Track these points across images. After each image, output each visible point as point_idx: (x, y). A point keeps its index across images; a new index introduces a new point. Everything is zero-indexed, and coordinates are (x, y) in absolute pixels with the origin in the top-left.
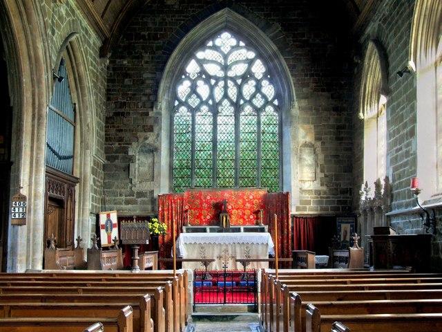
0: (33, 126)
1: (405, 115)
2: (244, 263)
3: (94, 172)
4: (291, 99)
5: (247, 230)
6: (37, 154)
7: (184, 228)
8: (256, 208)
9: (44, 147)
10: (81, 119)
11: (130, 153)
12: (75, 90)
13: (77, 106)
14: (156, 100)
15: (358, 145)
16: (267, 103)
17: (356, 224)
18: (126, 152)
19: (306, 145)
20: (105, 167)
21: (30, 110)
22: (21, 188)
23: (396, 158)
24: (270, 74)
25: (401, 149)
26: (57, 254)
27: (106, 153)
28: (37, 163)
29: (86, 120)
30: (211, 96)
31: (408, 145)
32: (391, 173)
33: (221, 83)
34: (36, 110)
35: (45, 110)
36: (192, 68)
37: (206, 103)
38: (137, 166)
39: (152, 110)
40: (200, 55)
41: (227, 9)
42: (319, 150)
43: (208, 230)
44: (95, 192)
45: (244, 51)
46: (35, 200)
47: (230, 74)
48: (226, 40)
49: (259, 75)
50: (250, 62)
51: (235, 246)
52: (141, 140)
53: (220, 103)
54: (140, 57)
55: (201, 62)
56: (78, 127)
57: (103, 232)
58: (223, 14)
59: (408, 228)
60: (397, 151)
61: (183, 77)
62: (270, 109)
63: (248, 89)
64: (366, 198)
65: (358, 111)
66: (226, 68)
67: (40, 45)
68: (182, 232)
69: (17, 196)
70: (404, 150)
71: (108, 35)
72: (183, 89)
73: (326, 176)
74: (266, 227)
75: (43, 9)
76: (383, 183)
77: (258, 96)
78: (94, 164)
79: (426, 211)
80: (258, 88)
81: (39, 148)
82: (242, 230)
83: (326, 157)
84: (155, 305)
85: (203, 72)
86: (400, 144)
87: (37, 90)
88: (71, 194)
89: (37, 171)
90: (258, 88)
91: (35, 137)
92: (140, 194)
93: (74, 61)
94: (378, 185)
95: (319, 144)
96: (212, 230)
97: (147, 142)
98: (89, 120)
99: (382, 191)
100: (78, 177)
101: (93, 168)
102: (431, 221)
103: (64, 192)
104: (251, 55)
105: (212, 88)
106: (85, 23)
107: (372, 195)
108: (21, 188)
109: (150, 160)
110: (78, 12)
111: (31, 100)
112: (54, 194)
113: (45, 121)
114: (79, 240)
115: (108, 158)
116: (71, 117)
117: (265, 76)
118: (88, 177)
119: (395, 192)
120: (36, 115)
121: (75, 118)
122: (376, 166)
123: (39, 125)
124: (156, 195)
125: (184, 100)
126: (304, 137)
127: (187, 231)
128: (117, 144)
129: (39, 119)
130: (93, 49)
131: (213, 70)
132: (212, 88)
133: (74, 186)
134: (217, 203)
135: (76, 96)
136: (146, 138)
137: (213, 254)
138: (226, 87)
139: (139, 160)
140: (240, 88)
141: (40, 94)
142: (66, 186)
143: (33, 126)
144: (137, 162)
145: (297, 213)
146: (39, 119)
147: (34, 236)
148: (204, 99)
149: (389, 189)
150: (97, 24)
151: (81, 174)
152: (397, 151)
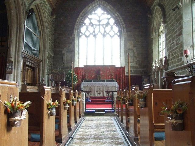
2: (108, 93)
5: (107, 81)
6: (19, 44)
8: (111, 73)
10: (43, 37)
11: (63, 52)
12: (40, 25)
13: (41, 31)
15: (150, 49)
17: (150, 79)
19: (130, 49)
20: (53, 58)
21: (16, 25)
22: (11, 58)
23: (171, 48)
24: (117, 23)
27: (54, 52)
29: (45, 37)
30: (94, 32)
31: (179, 39)
33: (98, 27)
34: (19, 25)
36: (87, 21)
38: (66, 57)
40: (90, 16)
42: (135, 51)
45: (106, 15)
46: (17, 63)
47: (101, 23)
48: (99, 11)
50: (109, 19)
51: (103, 88)
55: (90, 19)
57: (50, 81)
61: (83, 25)
64: (156, 67)
65: (150, 35)
66: (99, 21)
70: (175, 43)
71: (55, 7)
73: (138, 61)
74: (115, 80)
76: (164, 59)
78: (49, 55)
80: (112, 28)
85: (91, 23)
86: (173, 41)
90: (112, 28)
93: (39, 13)
95: (135, 49)
97: (69, 48)
98: (46, 38)
99: (164, 62)
100: (42, 59)
101: (48, 57)
102: (194, 69)
104: (109, 16)
108: (11, 58)
111: (16, 21)
115: (55, 54)
117: (114, 24)
119: (169, 62)
120: (19, 27)
122: (161, 50)
126: (129, 46)
127: (85, 82)
130: (48, 11)
135: (41, 28)
136: (69, 47)
137: (95, 90)
139: (66, 55)
143: (17, 32)
144: (66, 56)
146: (20, 29)
148: (91, 33)
149: (167, 61)
150: (51, 4)
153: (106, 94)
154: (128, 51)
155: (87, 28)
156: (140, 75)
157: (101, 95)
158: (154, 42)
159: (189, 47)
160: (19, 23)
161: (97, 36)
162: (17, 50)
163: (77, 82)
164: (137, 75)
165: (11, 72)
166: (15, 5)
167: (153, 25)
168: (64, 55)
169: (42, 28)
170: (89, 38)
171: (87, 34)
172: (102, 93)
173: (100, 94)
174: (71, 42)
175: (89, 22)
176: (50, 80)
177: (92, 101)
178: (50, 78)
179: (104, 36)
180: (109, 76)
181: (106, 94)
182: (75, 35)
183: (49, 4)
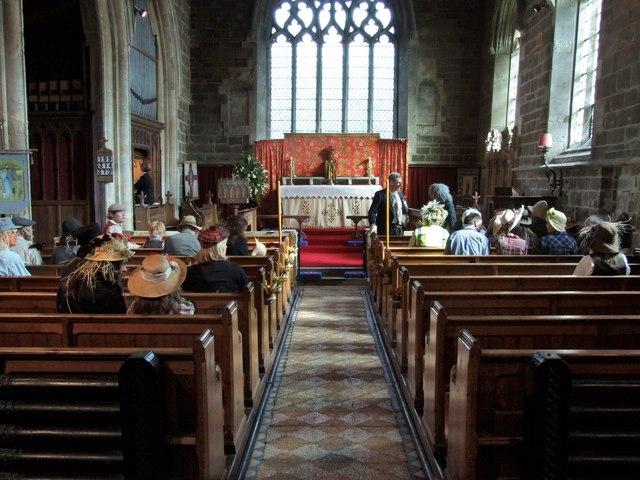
0: (114, 69)
1: (542, 68)
3: (180, 116)
6: (121, 102)
7: (284, 179)
9: (127, 93)
10: (163, 54)
11: (221, 92)
14: (249, 28)
16: (382, 31)
18: (216, 91)
19: (425, 83)
22: (105, 141)
25: (533, 96)
26: (149, 214)
28: (121, 112)
29: (169, 53)
30: (316, 22)
32: (520, 123)
34: (117, 51)
35: (127, 50)
37: (309, 30)
39: (245, 40)
43: (312, 182)
46: (121, 154)
53: (325, 31)
56: (160, 63)
59: (534, 186)
60: (529, 98)
62: (384, 38)
65: (488, 45)
68: (282, 184)
69: (102, 150)
73: (448, 120)
74: (377, 179)
77: (372, 22)
79: (553, 170)
81: (121, 95)
82: (350, 182)
84: (357, 377)
87: (115, 27)
88: (157, 143)
92: (234, 140)
94: (505, 134)
96: (316, 182)
97: (241, 78)
103: (148, 141)
105: (316, 12)
107: (497, 146)
108: (105, 141)
109: (244, 100)
111: (109, 39)
112: (142, 146)
113: (127, 63)
116: (153, 54)
118: (174, 122)
121: (154, 53)
123: (120, 69)
124: (251, 142)
125: (282, 26)
127: (288, 183)
128: (205, 81)
132: (316, 12)
133: (159, 133)
134: (325, 150)
135: (156, 26)
136: (239, 74)
140: (349, 11)
141: (120, 32)
142: (150, 134)
144: (229, 102)
145: (414, 163)
146: (120, 62)
147: (123, 194)
151: (165, 118)
152: (529, 98)
153: (349, 223)
154: (420, 90)
156: (450, 163)
157: (336, 224)
158: (497, 69)
159: (561, 121)
160: (117, 45)
161: (325, 37)
163: (266, 186)
167: (499, 13)
168: (222, 99)
169: (159, 27)
170: (299, 45)
171: (294, 29)
172: (337, 218)
173: (332, 219)
174: (245, 60)
176: (188, 179)
177: (310, 242)
178: (186, 174)
179: (347, 37)
180: (361, 167)
181: (349, 223)
182: (256, 38)
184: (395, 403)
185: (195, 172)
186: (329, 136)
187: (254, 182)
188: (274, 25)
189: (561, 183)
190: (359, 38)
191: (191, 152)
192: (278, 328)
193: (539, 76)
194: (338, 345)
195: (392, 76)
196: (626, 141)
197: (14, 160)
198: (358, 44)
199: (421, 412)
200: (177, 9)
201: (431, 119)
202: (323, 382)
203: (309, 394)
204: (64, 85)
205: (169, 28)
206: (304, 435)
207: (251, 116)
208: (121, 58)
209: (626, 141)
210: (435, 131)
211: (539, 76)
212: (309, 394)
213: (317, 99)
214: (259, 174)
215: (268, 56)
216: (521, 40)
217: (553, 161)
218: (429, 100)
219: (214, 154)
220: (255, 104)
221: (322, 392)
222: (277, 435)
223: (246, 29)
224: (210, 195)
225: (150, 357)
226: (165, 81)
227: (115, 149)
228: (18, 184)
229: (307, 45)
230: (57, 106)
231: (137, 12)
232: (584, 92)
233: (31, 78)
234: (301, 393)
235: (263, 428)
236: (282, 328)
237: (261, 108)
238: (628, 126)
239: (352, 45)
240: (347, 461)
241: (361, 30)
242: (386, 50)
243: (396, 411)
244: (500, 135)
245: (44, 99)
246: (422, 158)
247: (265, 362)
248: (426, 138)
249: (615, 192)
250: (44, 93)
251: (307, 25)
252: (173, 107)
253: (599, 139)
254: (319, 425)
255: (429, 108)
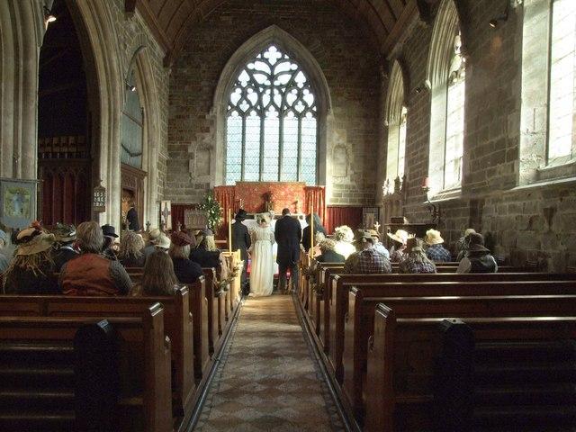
3: (159, 167)
4: (328, 106)
9: (119, 146)
11: (190, 151)
14: (212, 105)
16: (307, 109)
18: (186, 150)
19: (339, 146)
20: (168, 162)
24: (312, 84)
30: (260, 102)
31: (423, 150)
33: (268, 91)
35: (120, 115)
37: (255, 108)
41: (272, 28)
44: (160, 183)
46: (113, 191)
48: (273, 54)
49: (300, 85)
50: (293, 73)
52: (199, 139)
53: (267, 109)
54: (198, 67)
55: (251, 73)
57: (162, 216)
58: (270, 31)
62: (309, 115)
63: (291, 98)
66: (272, 77)
67: (114, 58)
70: (419, 154)
72: (235, 97)
73: (355, 173)
75: (117, 26)
77: (300, 103)
79: (433, 205)
80: (300, 96)
81: (115, 147)
83: (356, 156)
85: (252, 81)
87: (112, 99)
88: (141, 186)
89: (25, 115)
90: (300, 96)
91: (111, 138)
92: (198, 186)
94: (397, 181)
95: (350, 145)
104: (294, 67)
105: (260, 95)
106: (151, 37)
109: (206, 157)
110: (145, 27)
111: (107, 106)
114: (148, 224)
116: (140, 121)
117: (306, 85)
124: (211, 187)
125: (235, 105)
129: (114, 123)
131: (261, 79)
132: (260, 95)
136: (203, 138)
138: (272, 95)
140: (284, 95)
146: (114, 123)
152: (415, 154)
154: (335, 152)
155: (244, 95)
156: (357, 204)
161: (267, 113)
162: (21, 88)
163: (222, 219)
164: (351, 204)
165: (103, 209)
166: (107, 74)
168: (191, 156)
171: (245, 107)
175: (248, 79)
179: (282, 113)
183: (159, 43)
184: (320, 375)
185: (169, 210)
186: (269, 184)
187: (213, 216)
188: (230, 104)
189: (442, 214)
190: (291, 114)
191: (165, 195)
192: (227, 319)
193: (421, 138)
194: (272, 332)
195: (315, 140)
196: (488, 179)
197: (24, 187)
198: (290, 119)
199: (341, 382)
200: (159, 90)
201: (343, 172)
202: (261, 359)
203: (250, 368)
204: (71, 139)
205: (152, 103)
206: (244, 400)
207: (211, 169)
208: (115, 119)
209: (488, 179)
210: (347, 181)
211: (421, 138)
212: (250, 368)
213: (260, 157)
214: (217, 210)
215: (225, 125)
216: (408, 115)
217: (433, 199)
218: (342, 158)
219: (185, 196)
220: (214, 158)
221: (259, 367)
222: (221, 400)
223: (209, 106)
224: (179, 225)
225: (103, 324)
226: (148, 141)
227: (108, 189)
228: (25, 205)
229: (253, 119)
230: (66, 155)
231: (128, 88)
232: (454, 149)
233: (42, 134)
234: (243, 368)
235: (210, 396)
236: (230, 321)
237: (219, 163)
238: (489, 168)
239: (286, 120)
240: (279, 422)
241: (292, 108)
242: (310, 123)
243: (321, 382)
244: (394, 183)
245: (56, 150)
246: (337, 201)
247: (215, 344)
248: (341, 186)
249: (480, 218)
250: (57, 145)
251: (253, 104)
252: (154, 158)
253: (467, 180)
254: (258, 393)
255: (341, 164)
